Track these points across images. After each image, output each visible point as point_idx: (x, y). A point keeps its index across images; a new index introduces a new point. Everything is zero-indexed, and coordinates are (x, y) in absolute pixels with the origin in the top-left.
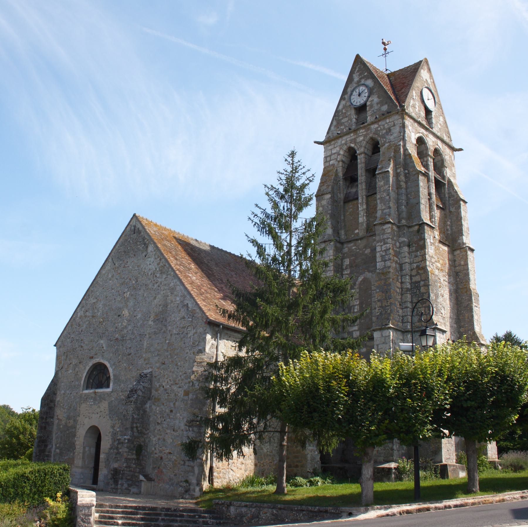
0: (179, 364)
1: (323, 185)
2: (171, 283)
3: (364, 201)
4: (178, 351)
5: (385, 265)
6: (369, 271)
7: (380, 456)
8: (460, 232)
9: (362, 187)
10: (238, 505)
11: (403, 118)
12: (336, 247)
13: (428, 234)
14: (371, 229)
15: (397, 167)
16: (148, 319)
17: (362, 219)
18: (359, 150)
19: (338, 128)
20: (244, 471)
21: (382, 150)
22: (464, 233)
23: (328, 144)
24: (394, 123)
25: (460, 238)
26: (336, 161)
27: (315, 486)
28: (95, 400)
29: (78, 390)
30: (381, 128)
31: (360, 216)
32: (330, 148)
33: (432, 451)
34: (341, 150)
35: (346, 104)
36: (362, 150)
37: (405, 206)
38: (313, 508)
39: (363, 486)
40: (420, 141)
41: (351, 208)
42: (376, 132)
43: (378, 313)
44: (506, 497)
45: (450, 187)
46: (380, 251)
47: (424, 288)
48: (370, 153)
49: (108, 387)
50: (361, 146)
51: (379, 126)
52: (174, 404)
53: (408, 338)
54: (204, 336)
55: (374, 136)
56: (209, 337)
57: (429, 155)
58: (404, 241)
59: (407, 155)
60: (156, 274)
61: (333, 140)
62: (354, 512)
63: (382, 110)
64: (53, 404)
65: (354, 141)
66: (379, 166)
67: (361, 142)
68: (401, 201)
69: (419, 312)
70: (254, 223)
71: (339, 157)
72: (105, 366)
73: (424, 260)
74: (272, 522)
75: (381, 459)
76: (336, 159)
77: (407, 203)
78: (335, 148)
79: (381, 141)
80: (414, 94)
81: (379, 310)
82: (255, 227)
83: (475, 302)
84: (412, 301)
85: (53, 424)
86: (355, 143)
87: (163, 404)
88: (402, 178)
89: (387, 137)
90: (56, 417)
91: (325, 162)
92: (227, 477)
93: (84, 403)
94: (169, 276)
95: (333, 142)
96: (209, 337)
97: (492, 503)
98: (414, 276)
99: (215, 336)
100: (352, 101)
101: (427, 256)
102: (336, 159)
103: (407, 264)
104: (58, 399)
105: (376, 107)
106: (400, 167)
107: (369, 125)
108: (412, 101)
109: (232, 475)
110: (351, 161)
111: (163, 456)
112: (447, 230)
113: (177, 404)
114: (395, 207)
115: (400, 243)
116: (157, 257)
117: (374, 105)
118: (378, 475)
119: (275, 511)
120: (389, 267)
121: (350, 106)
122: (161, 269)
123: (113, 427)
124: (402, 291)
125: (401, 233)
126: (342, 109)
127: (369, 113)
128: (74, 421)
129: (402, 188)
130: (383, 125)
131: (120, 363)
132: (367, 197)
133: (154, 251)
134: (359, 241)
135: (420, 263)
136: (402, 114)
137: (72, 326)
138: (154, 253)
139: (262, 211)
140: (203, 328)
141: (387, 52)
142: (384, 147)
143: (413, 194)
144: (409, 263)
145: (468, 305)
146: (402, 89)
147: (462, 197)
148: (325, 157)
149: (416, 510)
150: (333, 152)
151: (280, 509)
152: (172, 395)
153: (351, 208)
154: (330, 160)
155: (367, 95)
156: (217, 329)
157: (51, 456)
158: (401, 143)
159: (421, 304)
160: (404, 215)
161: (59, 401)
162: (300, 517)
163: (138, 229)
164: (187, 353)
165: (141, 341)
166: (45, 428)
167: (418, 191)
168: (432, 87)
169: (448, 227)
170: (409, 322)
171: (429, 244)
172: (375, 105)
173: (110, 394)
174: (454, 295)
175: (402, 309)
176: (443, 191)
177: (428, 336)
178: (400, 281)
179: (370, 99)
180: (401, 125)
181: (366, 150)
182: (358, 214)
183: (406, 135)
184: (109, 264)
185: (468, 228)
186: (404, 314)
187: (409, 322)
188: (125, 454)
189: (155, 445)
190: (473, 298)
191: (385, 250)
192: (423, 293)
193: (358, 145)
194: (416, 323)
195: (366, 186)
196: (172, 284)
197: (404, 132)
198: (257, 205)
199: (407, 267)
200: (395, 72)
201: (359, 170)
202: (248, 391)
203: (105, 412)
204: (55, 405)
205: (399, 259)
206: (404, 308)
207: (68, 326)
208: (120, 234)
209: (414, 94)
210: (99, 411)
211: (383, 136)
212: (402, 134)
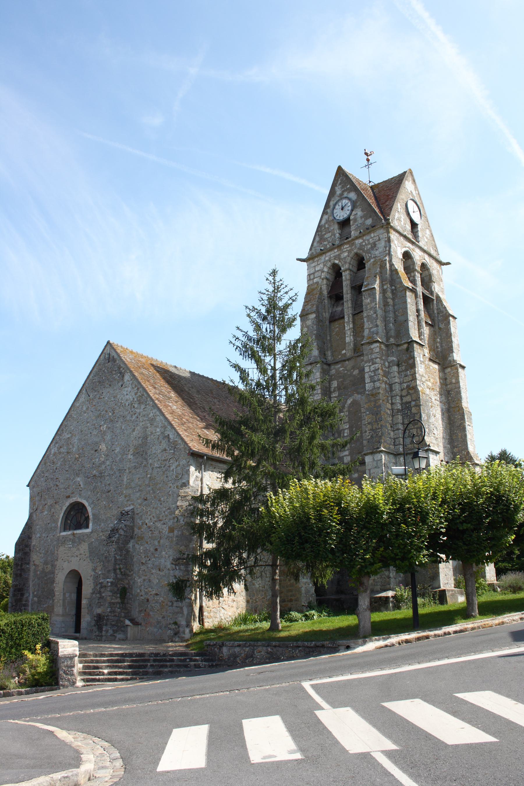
0: (162, 499)
1: (308, 304)
3: (351, 319)
4: (160, 486)
5: (374, 386)
6: (358, 393)
8: (450, 350)
10: (231, 645)
11: (388, 232)
12: (322, 369)
13: (418, 352)
18: (343, 267)
19: (321, 244)
23: (311, 261)
24: (379, 238)
25: (451, 355)
31: (347, 335)
32: (313, 265)
35: (329, 218)
36: (347, 266)
38: (309, 643)
40: (407, 256)
41: (337, 328)
42: (361, 247)
48: (355, 270)
49: (87, 527)
50: (346, 263)
51: (364, 241)
52: (159, 542)
54: (187, 468)
55: (359, 252)
56: (192, 469)
57: (416, 270)
58: (393, 361)
59: (394, 270)
61: (316, 257)
62: (352, 645)
65: (338, 257)
67: (345, 258)
70: (235, 347)
72: (83, 506)
73: (414, 379)
74: (267, 660)
75: (378, 588)
76: (320, 277)
77: (395, 320)
78: (318, 265)
79: (366, 256)
83: (468, 421)
84: (403, 422)
85: (29, 570)
86: (340, 259)
87: (147, 543)
88: (389, 294)
89: (372, 252)
90: (32, 563)
91: (309, 280)
94: (148, 406)
95: (316, 259)
96: (192, 469)
98: (404, 396)
100: (335, 215)
101: (417, 375)
102: (320, 277)
104: (34, 543)
105: (360, 221)
106: (386, 284)
107: (353, 240)
108: (397, 214)
109: (224, 614)
110: (336, 278)
113: (162, 541)
115: (388, 362)
116: (134, 386)
119: (269, 649)
121: (333, 220)
123: (94, 570)
124: (393, 412)
126: (325, 224)
127: (353, 228)
128: (52, 566)
130: (368, 240)
131: (100, 501)
132: (354, 315)
135: (410, 382)
138: (131, 382)
139: (244, 333)
140: (186, 460)
142: (369, 263)
145: (461, 424)
147: (451, 312)
148: (308, 275)
150: (317, 269)
151: (275, 646)
153: (337, 328)
154: (314, 278)
155: (350, 208)
156: (201, 460)
157: (28, 606)
158: (387, 258)
160: (392, 333)
161: (34, 546)
164: (170, 487)
165: (120, 476)
169: (438, 344)
171: (419, 362)
172: (359, 219)
175: (394, 431)
178: (390, 402)
179: (354, 213)
182: (345, 334)
183: (392, 250)
185: (458, 345)
186: (395, 437)
188: (109, 598)
189: (141, 586)
190: (466, 417)
191: (373, 371)
192: (414, 414)
195: (352, 304)
196: (152, 414)
197: (390, 246)
199: (397, 387)
200: (379, 184)
201: (344, 288)
203: (85, 555)
204: (30, 550)
211: (368, 252)
212: (387, 249)
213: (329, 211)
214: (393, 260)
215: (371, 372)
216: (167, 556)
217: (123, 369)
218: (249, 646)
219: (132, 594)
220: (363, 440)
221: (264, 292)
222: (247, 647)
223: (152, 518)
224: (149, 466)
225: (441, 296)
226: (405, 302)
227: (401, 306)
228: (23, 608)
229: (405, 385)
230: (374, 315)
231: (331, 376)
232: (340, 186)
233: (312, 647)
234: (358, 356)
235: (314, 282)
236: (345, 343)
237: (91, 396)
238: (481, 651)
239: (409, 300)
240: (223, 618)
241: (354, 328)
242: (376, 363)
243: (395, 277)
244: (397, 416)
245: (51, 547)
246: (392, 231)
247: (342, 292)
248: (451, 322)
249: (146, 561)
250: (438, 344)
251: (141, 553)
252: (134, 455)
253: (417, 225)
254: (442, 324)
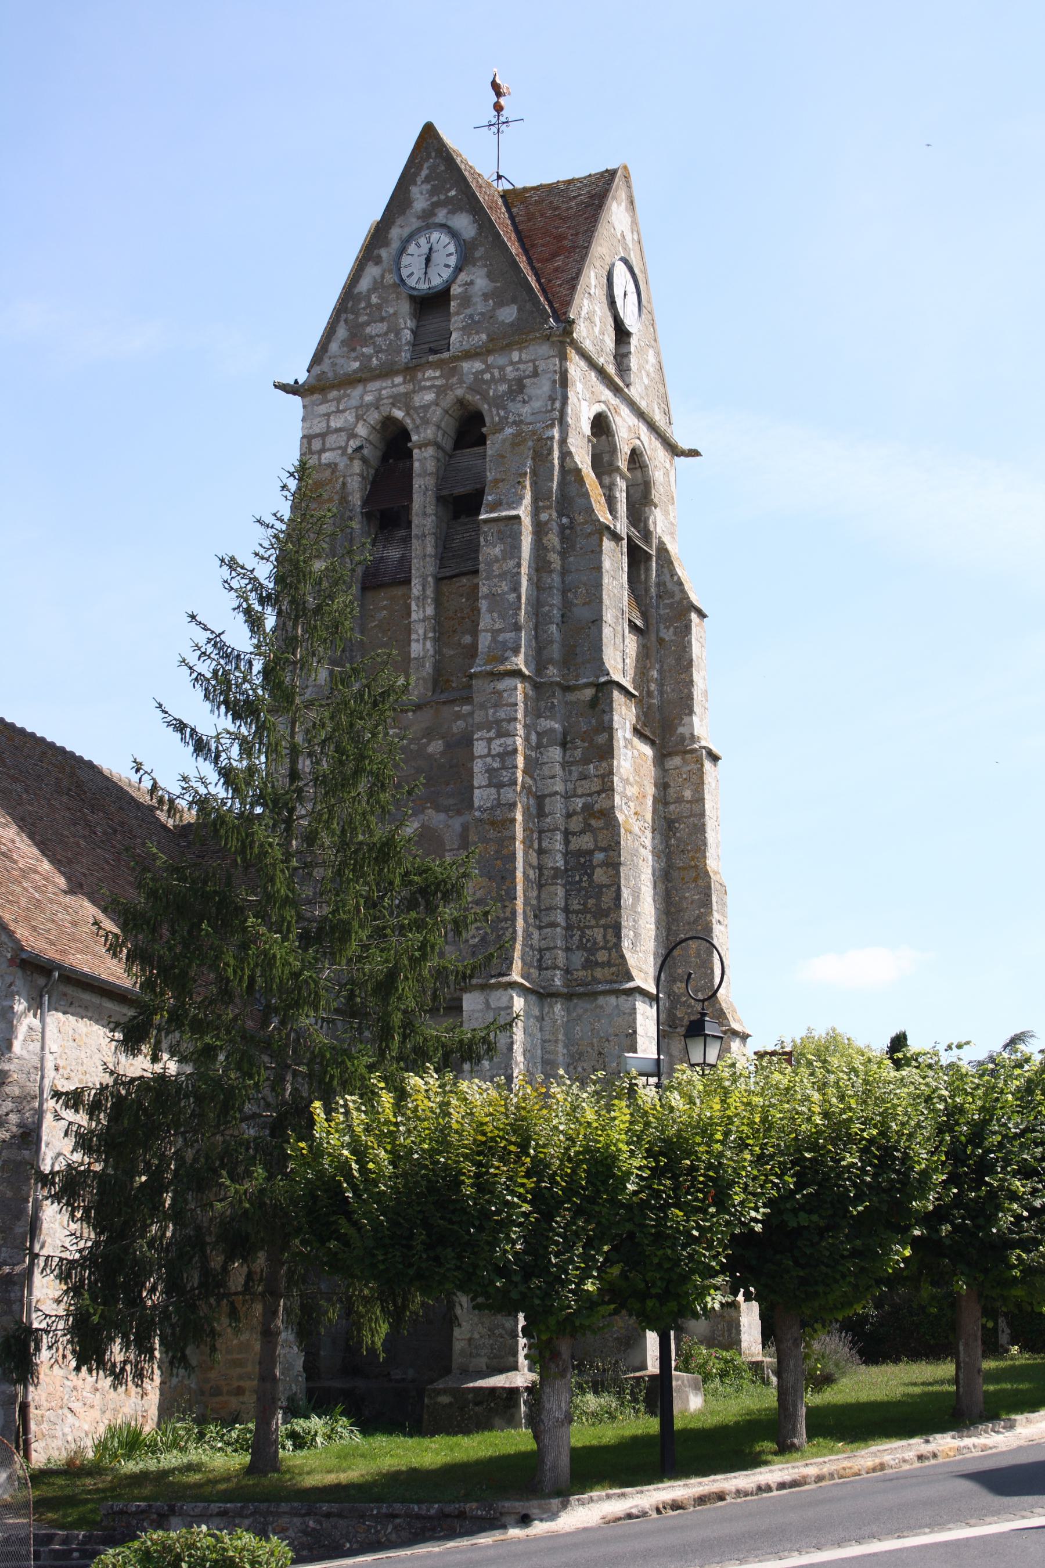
3: (429, 592)
6: (438, 809)
7: (478, 1355)
8: (685, 704)
9: (424, 547)
10: (197, 1511)
11: (564, 357)
13: (621, 715)
14: (448, 681)
15: (541, 504)
18: (418, 433)
19: (354, 350)
20: (99, 1412)
21: (493, 446)
22: (696, 709)
23: (316, 396)
24: (535, 368)
25: (686, 719)
27: (309, 1448)
30: (492, 374)
31: (414, 636)
32: (323, 409)
33: (617, 1339)
35: (383, 277)
36: (429, 433)
37: (557, 624)
38: (424, 1507)
39: (546, 1441)
40: (601, 425)
41: (384, 608)
42: (478, 385)
43: (474, 937)
44: (887, 1458)
45: (662, 567)
46: (485, 756)
47: (605, 873)
48: (448, 445)
50: (426, 422)
51: (488, 368)
53: (554, 1013)
54: (6, 1003)
55: (469, 397)
56: (20, 1006)
57: (618, 469)
58: (552, 730)
59: (570, 471)
61: (333, 387)
62: (534, 1511)
63: (501, 318)
65: (404, 400)
66: (490, 498)
67: (426, 407)
68: (547, 608)
69: (588, 941)
70: (194, 675)
71: (351, 443)
73: (608, 789)
74: (305, 1553)
75: (482, 1362)
76: (344, 449)
77: (563, 616)
78: (338, 411)
79: (492, 416)
80: (593, 282)
81: (478, 929)
82: (197, 686)
83: (718, 911)
84: (567, 905)
86: (408, 409)
88: (553, 539)
89: (511, 406)
92: (59, 1434)
95: (333, 394)
96: (20, 1006)
97: (859, 1475)
98: (574, 834)
99: (36, 1004)
100: (405, 273)
101: (616, 779)
102: (344, 449)
103: (558, 797)
105: (480, 307)
106: (549, 507)
107: (456, 358)
108: (586, 302)
109: (72, 1426)
110: (385, 458)
112: (650, 694)
114: (531, 625)
115: (538, 734)
118: (477, 1409)
119: (311, 1523)
121: (395, 285)
124: (541, 875)
125: (542, 704)
126: (370, 292)
127: (456, 322)
129: (551, 572)
130: (502, 369)
132: (439, 580)
135: (595, 797)
136: (561, 342)
139: (211, 637)
141: (502, 119)
142: (500, 437)
143: (582, 590)
144: (562, 796)
145: (699, 917)
146: (554, 255)
147: (695, 598)
149: (694, 1500)
150: (333, 424)
151: (328, 1515)
153: (384, 608)
154: (323, 450)
155: (453, 261)
156: (41, 981)
158: (556, 433)
159: (594, 917)
160: (555, 651)
162: (385, 1535)
167: (599, 586)
169: (653, 686)
170: (559, 968)
171: (622, 743)
172: (477, 299)
174: (660, 885)
175: (540, 928)
176: (643, 577)
177: (708, 1039)
178: (536, 846)
179: (463, 277)
181: (440, 434)
182: (408, 630)
183: (569, 411)
185: (705, 693)
187: (559, 968)
190: (714, 899)
191: (499, 755)
192: (601, 887)
193: (415, 416)
194: (577, 970)
195: (436, 547)
197: (565, 399)
198: (193, 617)
199: (559, 805)
200: (525, 190)
201: (415, 496)
202: (228, 1183)
205: (535, 780)
206: (546, 927)
209: (592, 279)
211: (499, 402)
212: (558, 405)
213: (384, 253)
214: (570, 440)
215: (493, 756)
218: (252, 1514)
221: (271, 520)
222: (247, 1517)
225: (669, 547)
226: (598, 568)
227: (584, 579)
229: (579, 803)
232: (427, 187)
233: (430, 1518)
234: (444, 703)
235: (323, 461)
238: (913, 1528)
239: (607, 564)
240: (70, 1438)
243: (573, 490)
246: (572, 354)
247: (408, 509)
248: (693, 624)
250: (653, 686)
253: (628, 334)
254: (668, 628)
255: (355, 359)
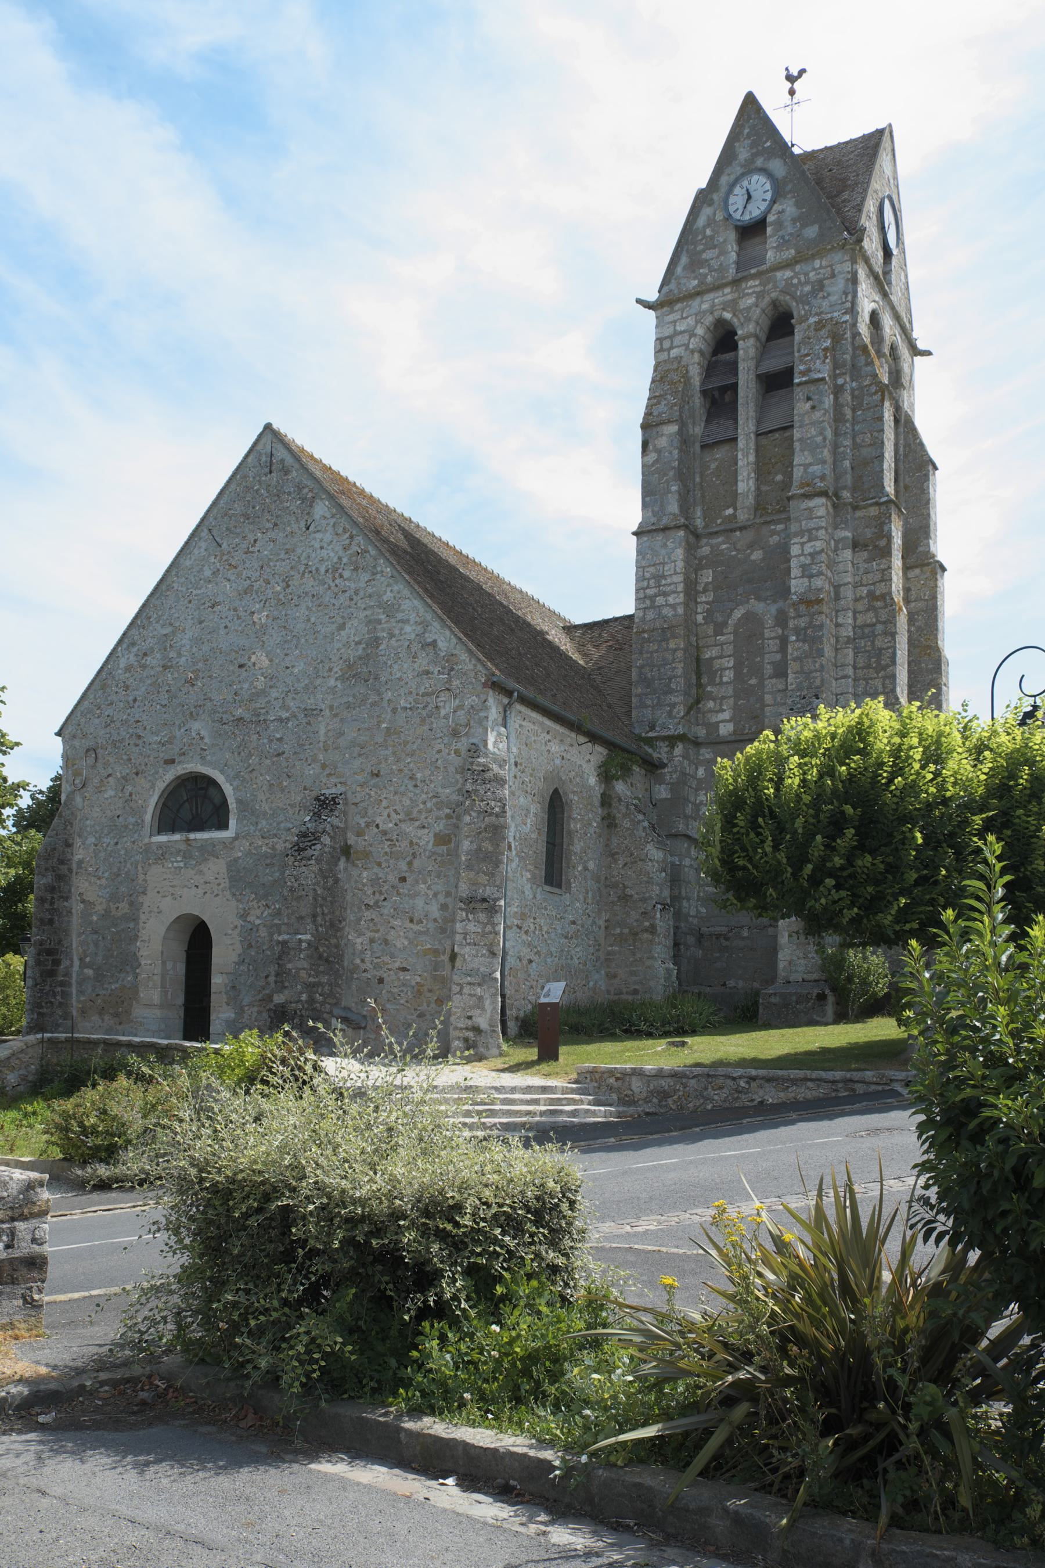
0: (419, 775)
1: (659, 403)
2: (386, 592)
3: (752, 445)
4: (415, 747)
5: (810, 586)
6: (759, 599)
12: (688, 543)
16: (326, 674)
17: (746, 484)
23: (665, 309)
24: (833, 271)
26: (686, 350)
28: (187, 856)
29: (136, 836)
30: (799, 279)
31: (740, 478)
32: (671, 318)
34: (699, 325)
36: (751, 327)
42: (788, 289)
46: (799, 555)
48: (764, 338)
49: (223, 825)
50: (748, 319)
52: (410, 864)
58: (846, 538)
60: (340, 571)
61: (679, 300)
64: (66, 867)
65: (732, 305)
67: (749, 309)
71: (692, 340)
72: (212, 782)
76: (687, 346)
78: (683, 318)
85: (70, 912)
87: (379, 864)
89: (814, 302)
90: (75, 898)
91: (659, 351)
93: (156, 863)
94: (378, 576)
95: (679, 306)
98: (860, 612)
102: (687, 346)
104: (80, 857)
111: (385, 975)
113: (416, 863)
116: (340, 531)
117: (785, 224)
120: (820, 590)
122: (354, 559)
123: (244, 916)
124: (837, 641)
126: (705, 227)
127: (772, 242)
128: (131, 904)
130: (806, 274)
131: (254, 774)
133: (333, 516)
134: (738, 533)
137: (104, 687)
138: (332, 521)
140: (478, 696)
141: (795, 101)
148: (657, 339)
150: (678, 328)
152: (404, 844)
154: (671, 348)
155: (768, 196)
157: (70, 985)
161: (80, 862)
163: (282, 461)
164: (439, 751)
165: (309, 723)
166: (51, 922)
168: (895, 197)
173: (231, 843)
175: (836, 679)
179: (777, 207)
180: (849, 276)
184: (203, 545)
186: (839, 691)
188: (303, 974)
189: (362, 952)
191: (810, 554)
192: (880, 650)
193: (740, 316)
196: (389, 593)
200: (814, 151)
203: (219, 884)
204: (70, 870)
207: (93, 688)
208: (230, 473)
210: (202, 881)
211: (804, 300)
212: (850, 298)
213: (715, 197)
216: (430, 893)
217: (311, 490)
219: (343, 968)
220: (763, 693)
223: (393, 815)
224: (385, 704)
228: (59, 989)
229: (864, 591)
230: (819, 439)
231: (701, 559)
232: (747, 142)
235: (672, 356)
236: (735, 494)
237: (224, 546)
241: (757, 462)
242: (816, 539)
244: (846, 651)
245: (128, 866)
249: (377, 902)
251: (364, 885)
252: (342, 678)
255: (694, 279)
